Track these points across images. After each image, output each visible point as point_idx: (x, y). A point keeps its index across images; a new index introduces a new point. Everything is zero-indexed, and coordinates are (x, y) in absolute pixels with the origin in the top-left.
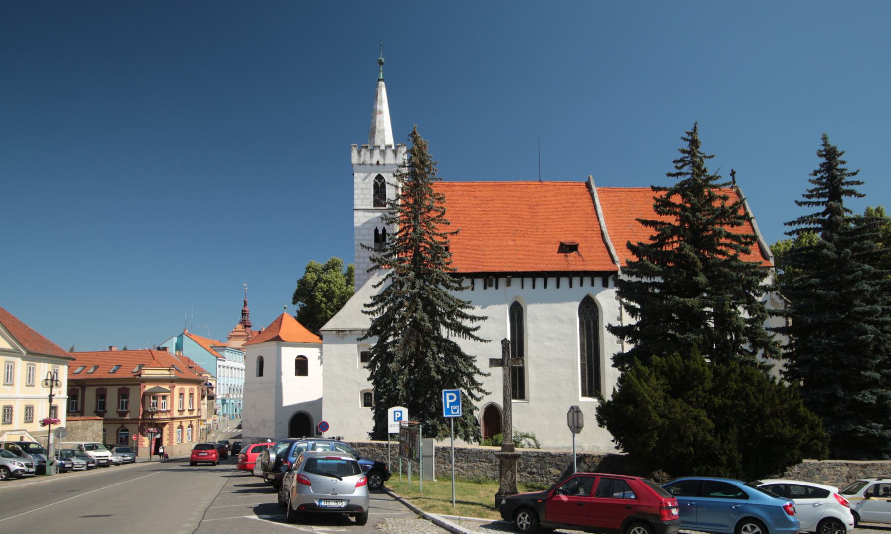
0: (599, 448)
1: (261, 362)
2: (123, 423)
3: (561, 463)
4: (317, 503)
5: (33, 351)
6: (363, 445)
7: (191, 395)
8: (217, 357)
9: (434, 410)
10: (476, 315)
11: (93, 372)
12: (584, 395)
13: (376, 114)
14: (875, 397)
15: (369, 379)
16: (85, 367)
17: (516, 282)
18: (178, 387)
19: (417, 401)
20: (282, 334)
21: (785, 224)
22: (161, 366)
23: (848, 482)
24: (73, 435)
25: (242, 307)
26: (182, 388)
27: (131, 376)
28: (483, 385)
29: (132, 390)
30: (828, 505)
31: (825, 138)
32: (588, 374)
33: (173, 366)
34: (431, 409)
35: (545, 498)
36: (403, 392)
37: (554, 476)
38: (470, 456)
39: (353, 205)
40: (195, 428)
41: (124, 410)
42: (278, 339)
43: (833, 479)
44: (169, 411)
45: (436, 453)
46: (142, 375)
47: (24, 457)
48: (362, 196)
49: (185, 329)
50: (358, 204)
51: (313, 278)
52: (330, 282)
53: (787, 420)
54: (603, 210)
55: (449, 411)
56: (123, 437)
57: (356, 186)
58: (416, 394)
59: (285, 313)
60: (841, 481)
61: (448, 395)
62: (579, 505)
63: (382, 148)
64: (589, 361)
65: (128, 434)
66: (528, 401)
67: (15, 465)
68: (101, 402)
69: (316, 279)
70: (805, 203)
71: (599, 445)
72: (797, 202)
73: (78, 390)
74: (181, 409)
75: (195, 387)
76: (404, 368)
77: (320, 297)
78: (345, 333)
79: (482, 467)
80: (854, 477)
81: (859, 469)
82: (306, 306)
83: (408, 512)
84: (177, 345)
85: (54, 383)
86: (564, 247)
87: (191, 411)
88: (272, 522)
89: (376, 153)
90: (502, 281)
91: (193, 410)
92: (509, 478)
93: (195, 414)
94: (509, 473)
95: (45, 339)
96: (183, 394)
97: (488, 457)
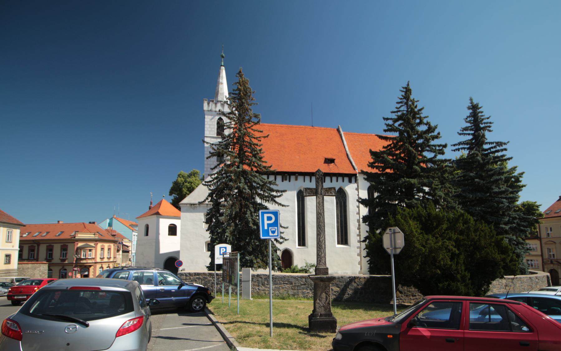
0: (347, 273)
1: (147, 227)
2: (64, 266)
3: (340, 283)
6: (204, 274)
7: (109, 249)
8: (133, 230)
9: (251, 249)
10: (279, 189)
11: (46, 235)
12: (338, 243)
13: (219, 84)
15: (207, 231)
16: (41, 232)
17: (301, 178)
18: (100, 245)
19: (239, 243)
20: (160, 211)
21: (452, 145)
22: (90, 232)
23: (506, 289)
24: (24, 273)
25: (149, 205)
27: (69, 237)
28: (284, 234)
29: (70, 246)
31: (471, 99)
32: (341, 231)
34: (249, 249)
35: (397, 332)
36: (230, 238)
37: (335, 292)
38: (277, 280)
41: (64, 258)
42: (158, 214)
44: (93, 259)
45: (252, 279)
46: (76, 237)
48: (209, 129)
49: (114, 215)
50: (207, 133)
51: (182, 181)
52: (191, 183)
53: (496, 249)
54: (347, 143)
55: (266, 232)
56: (64, 274)
57: (206, 123)
58: (239, 240)
59: (163, 199)
60: (502, 289)
61: (266, 216)
62: (448, 341)
64: (341, 224)
65: (66, 272)
66: (308, 247)
68: (50, 253)
69: (183, 181)
70: (462, 134)
71: (347, 272)
72: (458, 133)
73: (35, 246)
74: (109, 257)
76: (232, 222)
77: (185, 191)
78: (196, 206)
79: (286, 288)
82: (177, 197)
83: (220, 344)
86: (327, 160)
87: (109, 258)
89: (219, 105)
90: (293, 178)
92: (324, 300)
93: (112, 260)
94: (324, 295)
95: (4, 213)
96: (110, 249)
97: (290, 281)
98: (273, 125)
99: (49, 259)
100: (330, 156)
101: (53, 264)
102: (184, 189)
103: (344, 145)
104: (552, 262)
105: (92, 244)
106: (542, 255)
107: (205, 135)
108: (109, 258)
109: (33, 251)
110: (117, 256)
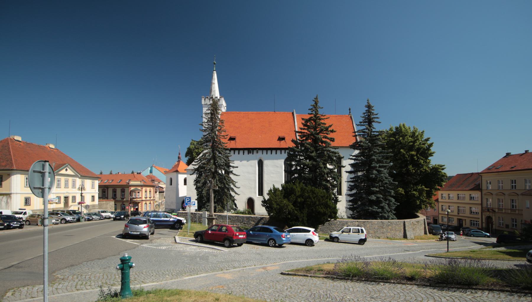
4: (130, 232)
5: (83, 175)
7: (150, 191)
13: (212, 84)
14: (375, 197)
18: (144, 189)
22: (138, 180)
25: (178, 155)
26: (146, 189)
27: (126, 184)
29: (126, 189)
30: (309, 235)
33: (143, 180)
40: (152, 204)
42: (177, 171)
44: (141, 198)
47: (73, 216)
49: (153, 165)
51: (193, 147)
56: (123, 207)
67: (69, 218)
70: (359, 125)
73: (105, 189)
75: (152, 188)
77: (195, 155)
84: (150, 171)
85: (83, 189)
88: (123, 240)
90: (255, 151)
91: (151, 197)
93: (152, 199)
98: (247, 112)
99: (114, 197)
100: (282, 135)
101: (117, 201)
102: (194, 154)
103: (295, 125)
104: (488, 211)
105: (140, 188)
106: (482, 204)
108: (150, 198)
109: (105, 192)
110: (156, 196)
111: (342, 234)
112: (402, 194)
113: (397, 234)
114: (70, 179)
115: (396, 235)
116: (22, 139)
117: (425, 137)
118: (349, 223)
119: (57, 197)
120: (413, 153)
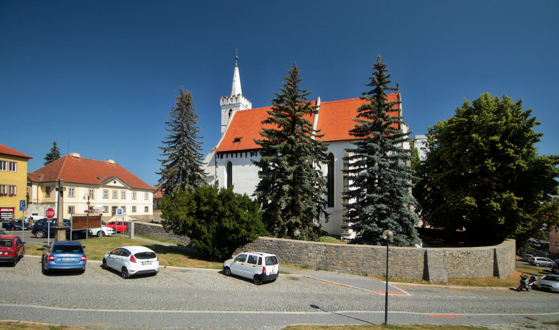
23: (325, 255)
39: (221, 124)
43: (316, 252)
48: (224, 120)
63: (236, 96)
80: (329, 253)
81: (333, 248)
107: (222, 125)
111: (235, 263)
112: (473, 207)
113: (408, 272)
114: (119, 191)
115: (406, 273)
116: (80, 156)
117: (523, 110)
118: (311, 248)
119: (104, 206)
120: (496, 138)
